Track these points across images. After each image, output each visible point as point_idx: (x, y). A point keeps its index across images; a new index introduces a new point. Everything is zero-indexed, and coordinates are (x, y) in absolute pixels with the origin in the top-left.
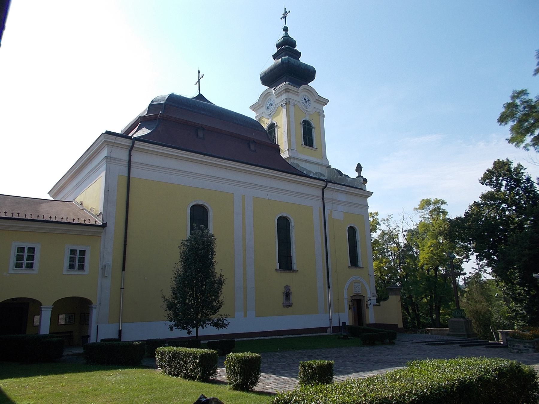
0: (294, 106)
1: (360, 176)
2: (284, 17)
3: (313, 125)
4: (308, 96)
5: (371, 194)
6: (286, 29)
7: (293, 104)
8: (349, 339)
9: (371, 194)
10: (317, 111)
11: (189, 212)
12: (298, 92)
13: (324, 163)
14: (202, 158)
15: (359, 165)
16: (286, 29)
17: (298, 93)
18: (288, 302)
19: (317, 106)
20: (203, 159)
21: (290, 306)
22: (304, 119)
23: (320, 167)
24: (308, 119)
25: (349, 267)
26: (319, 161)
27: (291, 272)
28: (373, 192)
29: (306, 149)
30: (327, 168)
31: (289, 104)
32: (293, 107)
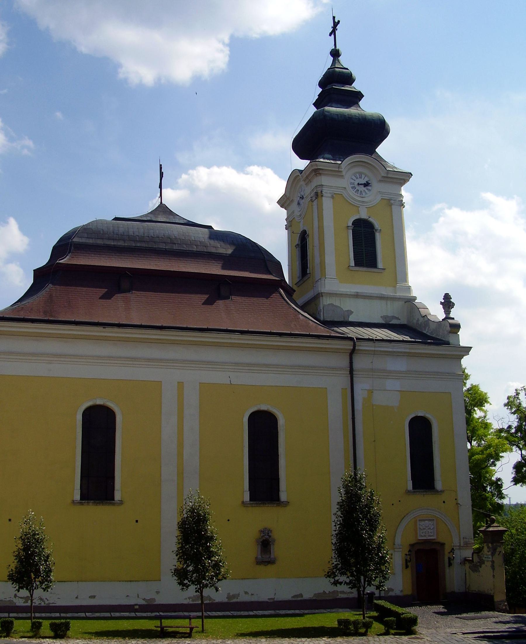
0: (333, 197)
1: (447, 318)
2: (333, 32)
3: (377, 225)
4: (364, 174)
5: (467, 350)
6: (335, 54)
7: (330, 195)
8: (189, 598)
9: (467, 350)
10: (387, 197)
11: (79, 417)
12: (340, 170)
13: (399, 294)
14: (101, 332)
15: (447, 297)
16: (335, 54)
17: (341, 171)
18: (268, 556)
19: (388, 188)
20: (104, 332)
21: (271, 562)
22: (357, 217)
23: (389, 302)
24: (364, 215)
25: (408, 492)
26: (388, 291)
27: (275, 505)
28: (471, 348)
29: (359, 272)
30: (405, 302)
31: (322, 196)
32: (332, 200)
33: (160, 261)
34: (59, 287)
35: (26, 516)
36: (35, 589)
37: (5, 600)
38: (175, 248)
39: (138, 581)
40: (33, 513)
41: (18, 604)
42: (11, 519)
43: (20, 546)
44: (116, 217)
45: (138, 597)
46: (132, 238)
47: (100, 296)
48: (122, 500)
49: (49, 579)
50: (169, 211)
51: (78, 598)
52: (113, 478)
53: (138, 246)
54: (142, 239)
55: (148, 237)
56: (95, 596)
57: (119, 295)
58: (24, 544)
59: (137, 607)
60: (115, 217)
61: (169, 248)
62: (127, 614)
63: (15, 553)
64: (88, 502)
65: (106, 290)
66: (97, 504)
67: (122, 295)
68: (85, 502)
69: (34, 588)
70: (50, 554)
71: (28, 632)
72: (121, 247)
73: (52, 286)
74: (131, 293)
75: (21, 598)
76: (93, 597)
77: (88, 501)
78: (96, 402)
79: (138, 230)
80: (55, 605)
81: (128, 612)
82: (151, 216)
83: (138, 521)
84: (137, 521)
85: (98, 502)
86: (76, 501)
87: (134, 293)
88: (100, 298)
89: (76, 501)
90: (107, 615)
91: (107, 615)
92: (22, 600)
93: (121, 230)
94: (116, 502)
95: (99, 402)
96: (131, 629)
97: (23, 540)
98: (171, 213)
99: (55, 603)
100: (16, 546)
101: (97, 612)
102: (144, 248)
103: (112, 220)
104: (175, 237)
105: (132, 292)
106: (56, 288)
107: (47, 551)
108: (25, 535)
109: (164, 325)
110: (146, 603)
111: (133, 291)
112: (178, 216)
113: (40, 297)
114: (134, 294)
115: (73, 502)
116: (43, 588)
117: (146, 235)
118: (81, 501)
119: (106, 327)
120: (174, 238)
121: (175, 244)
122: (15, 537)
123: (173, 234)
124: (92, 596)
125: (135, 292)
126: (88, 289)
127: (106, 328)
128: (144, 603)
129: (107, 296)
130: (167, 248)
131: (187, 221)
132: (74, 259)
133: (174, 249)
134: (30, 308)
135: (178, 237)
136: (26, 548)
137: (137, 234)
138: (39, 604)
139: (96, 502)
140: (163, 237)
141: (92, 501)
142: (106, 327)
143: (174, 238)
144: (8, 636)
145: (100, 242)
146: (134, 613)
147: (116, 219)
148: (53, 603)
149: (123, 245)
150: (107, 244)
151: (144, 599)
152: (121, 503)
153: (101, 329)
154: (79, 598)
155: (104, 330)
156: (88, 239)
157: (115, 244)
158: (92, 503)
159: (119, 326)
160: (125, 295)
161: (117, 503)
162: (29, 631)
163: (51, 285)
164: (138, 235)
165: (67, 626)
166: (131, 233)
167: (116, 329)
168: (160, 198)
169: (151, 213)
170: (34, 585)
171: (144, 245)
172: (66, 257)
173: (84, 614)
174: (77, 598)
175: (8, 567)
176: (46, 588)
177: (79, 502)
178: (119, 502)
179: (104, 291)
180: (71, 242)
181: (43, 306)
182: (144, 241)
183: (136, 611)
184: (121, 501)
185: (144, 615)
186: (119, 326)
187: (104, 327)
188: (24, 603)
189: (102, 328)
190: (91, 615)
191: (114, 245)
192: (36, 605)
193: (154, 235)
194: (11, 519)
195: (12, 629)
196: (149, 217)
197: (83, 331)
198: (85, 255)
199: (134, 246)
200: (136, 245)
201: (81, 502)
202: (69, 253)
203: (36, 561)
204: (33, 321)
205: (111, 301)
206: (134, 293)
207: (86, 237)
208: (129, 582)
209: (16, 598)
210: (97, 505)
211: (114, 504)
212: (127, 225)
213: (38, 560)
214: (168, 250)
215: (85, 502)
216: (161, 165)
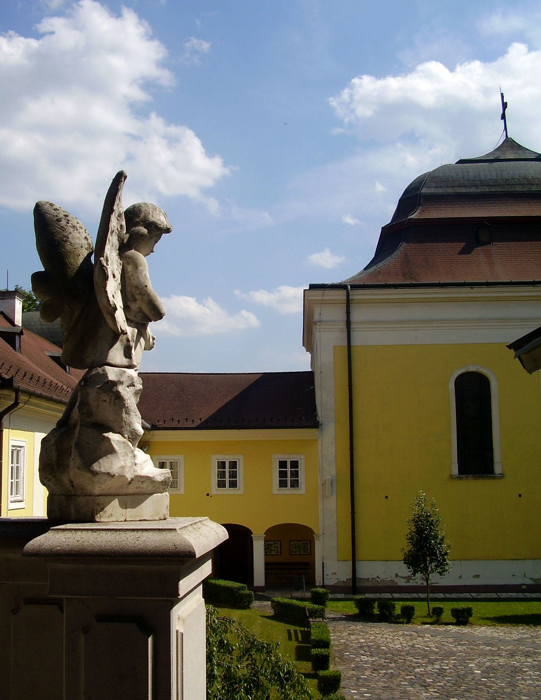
11: (452, 386)
20: (471, 292)
33: (519, 206)
34: (414, 245)
35: (417, 498)
36: (431, 572)
37: (386, 580)
38: (534, 190)
39: (523, 559)
40: (424, 494)
41: (399, 584)
42: (387, 497)
43: (414, 529)
44: (461, 159)
45: (525, 576)
46: (483, 183)
47: (459, 251)
48: (503, 473)
49: (445, 563)
50: (517, 145)
51: (461, 577)
52: (491, 449)
53: (493, 192)
54: (495, 183)
55: (502, 179)
56: (479, 576)
57: (478, 248)
58: (417, 526)
59: (524, 587)
60: (459, 159)
61: (527, 190)
62: (514, 595)
63: (408, 536)
64: (467, 477)
65: (464, 244)
66: (476, 478)
67: (482, 248)
68: (464, 477)
69: (429, 572)
70: (443, 536)
71: (425, 617)
72: (473, 193)
73: (406, 244)
74: (491, 245)
75: (402, 577)
76: (477, 576)
77: (467, 476)
78: (468, 369)
79: (490, 174)
80: (438, 585)
81: (515, 593)
82: (498, 153)
83: (522, 495)
84: (520, 496)
85: (477, 476)
86: (454, 476)
87: (495, 245)
88: (459, 253)
89: (455, 475)
90: (494, 595)
91: (494, 595)
92: (403, 579)
93: (471, 175)
94: (496, 475)
95: (472, 369)
96: (530, 613)
97: (416, 522)
98: (519, 147)
99: (437, 583)
100: (409, 529)
101: (482, 593)
102: (500, 193)
103: (456, 163)
104: (532, 177)
105: (492, 244)
106: (410, 246)
107: (440, 535)
108: (418, 518)
109: (536, 280)
110: (533, 583)
111: (493, 243)
112: (528, 151)
113: (396, 258)
114: (495, 246)
115: (452, 477)
116: (439, 572)
117: (499, 178)
118: (460, 476)
119: (473, 287)
120: (531, 177)
121: (533, 184)
122: (408, 520)
123: (530, 174)
124: (476, 575)
125: (496, 243)
126: (445, 244)
127: (474, 288)
128: (531, 582)
129: (466, 251)
130: (524, 190)
131: (538, 154)
132: (425, 213)
133: (533, 191)
134: (387, 271)
135: (535, 176)
136: (419, 531)
137: (489, 177)
138: (422, 584)
139: (476, 476)
140: (519, 178)
141: (471, 476)
142: (473, 287)
143: (531, 177)
144: (408, 622)
145: (450, 191)
146: (521, 594)
147: (461, 162)
148: (436, 583)
149: (476, 191)
150: (458, 192)
151: (532, 579)
152: (502, 476)
153: (468, 289)
154: (462, 577)
155: (472, 290)
156: (437, 188)
157: (467, 191)
158: (471, 477)
159: (488, 284)
160: (485, 248)
161: (498, 476)
162: (426, 616)
163: (404, 244)
164: (490, 178)
165: (468, 612)
166: (483, 177)
167: (485, 289)
168: (505, 132)
169: (498, 149)
170: (430, 569)
171: (499, 189)
172: (416, 211)
173: (469, 594)
174: (460, 577)
175: (401, 550)
176: (442, 572)
177: (458, 477)
178: (500, 475)
179: (462, 245)
180: (420, 193)
181: (400, 268)
182: (499, 185)
183: (523, 591)
184: (502, 474)
185: (534, 595)
186: (488, 284)
187: (471, 288)
188: (406, 582)
189: (470, 288)
190: (476, 596)
191: (466, 192)
192: (418, 584)
193: (508, 177)
194: (387, 497)
195: (413, 614)
196: (495, 154)
197: (449, 293)
198: (436, 206)
199: (487, 192)
200: (490, 191)
201: (460, 477)
202: (419, 206)
203: (432, 545)
204: (396, 286)
205: (471, 256)
206: (495, 245)
207: (435, 186)
208: (515, 561)
209: (397, 578)
210: (476, 479)
211: (494, 478)
212: (477, 168)
213: (435, 544)
214: (526, 192)
215: (464, 477)
216: (502, 94)
